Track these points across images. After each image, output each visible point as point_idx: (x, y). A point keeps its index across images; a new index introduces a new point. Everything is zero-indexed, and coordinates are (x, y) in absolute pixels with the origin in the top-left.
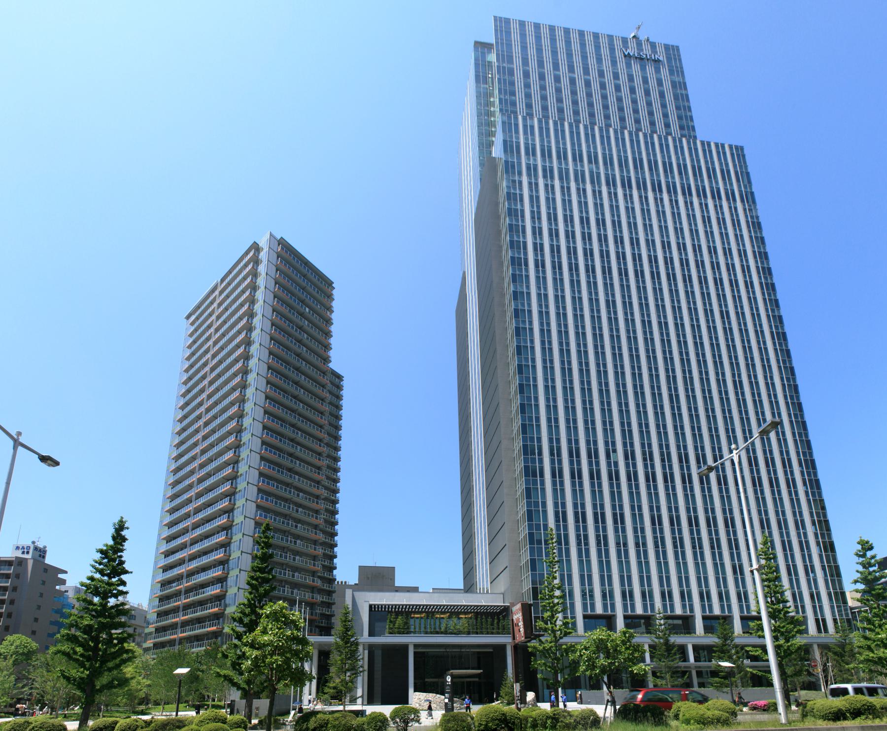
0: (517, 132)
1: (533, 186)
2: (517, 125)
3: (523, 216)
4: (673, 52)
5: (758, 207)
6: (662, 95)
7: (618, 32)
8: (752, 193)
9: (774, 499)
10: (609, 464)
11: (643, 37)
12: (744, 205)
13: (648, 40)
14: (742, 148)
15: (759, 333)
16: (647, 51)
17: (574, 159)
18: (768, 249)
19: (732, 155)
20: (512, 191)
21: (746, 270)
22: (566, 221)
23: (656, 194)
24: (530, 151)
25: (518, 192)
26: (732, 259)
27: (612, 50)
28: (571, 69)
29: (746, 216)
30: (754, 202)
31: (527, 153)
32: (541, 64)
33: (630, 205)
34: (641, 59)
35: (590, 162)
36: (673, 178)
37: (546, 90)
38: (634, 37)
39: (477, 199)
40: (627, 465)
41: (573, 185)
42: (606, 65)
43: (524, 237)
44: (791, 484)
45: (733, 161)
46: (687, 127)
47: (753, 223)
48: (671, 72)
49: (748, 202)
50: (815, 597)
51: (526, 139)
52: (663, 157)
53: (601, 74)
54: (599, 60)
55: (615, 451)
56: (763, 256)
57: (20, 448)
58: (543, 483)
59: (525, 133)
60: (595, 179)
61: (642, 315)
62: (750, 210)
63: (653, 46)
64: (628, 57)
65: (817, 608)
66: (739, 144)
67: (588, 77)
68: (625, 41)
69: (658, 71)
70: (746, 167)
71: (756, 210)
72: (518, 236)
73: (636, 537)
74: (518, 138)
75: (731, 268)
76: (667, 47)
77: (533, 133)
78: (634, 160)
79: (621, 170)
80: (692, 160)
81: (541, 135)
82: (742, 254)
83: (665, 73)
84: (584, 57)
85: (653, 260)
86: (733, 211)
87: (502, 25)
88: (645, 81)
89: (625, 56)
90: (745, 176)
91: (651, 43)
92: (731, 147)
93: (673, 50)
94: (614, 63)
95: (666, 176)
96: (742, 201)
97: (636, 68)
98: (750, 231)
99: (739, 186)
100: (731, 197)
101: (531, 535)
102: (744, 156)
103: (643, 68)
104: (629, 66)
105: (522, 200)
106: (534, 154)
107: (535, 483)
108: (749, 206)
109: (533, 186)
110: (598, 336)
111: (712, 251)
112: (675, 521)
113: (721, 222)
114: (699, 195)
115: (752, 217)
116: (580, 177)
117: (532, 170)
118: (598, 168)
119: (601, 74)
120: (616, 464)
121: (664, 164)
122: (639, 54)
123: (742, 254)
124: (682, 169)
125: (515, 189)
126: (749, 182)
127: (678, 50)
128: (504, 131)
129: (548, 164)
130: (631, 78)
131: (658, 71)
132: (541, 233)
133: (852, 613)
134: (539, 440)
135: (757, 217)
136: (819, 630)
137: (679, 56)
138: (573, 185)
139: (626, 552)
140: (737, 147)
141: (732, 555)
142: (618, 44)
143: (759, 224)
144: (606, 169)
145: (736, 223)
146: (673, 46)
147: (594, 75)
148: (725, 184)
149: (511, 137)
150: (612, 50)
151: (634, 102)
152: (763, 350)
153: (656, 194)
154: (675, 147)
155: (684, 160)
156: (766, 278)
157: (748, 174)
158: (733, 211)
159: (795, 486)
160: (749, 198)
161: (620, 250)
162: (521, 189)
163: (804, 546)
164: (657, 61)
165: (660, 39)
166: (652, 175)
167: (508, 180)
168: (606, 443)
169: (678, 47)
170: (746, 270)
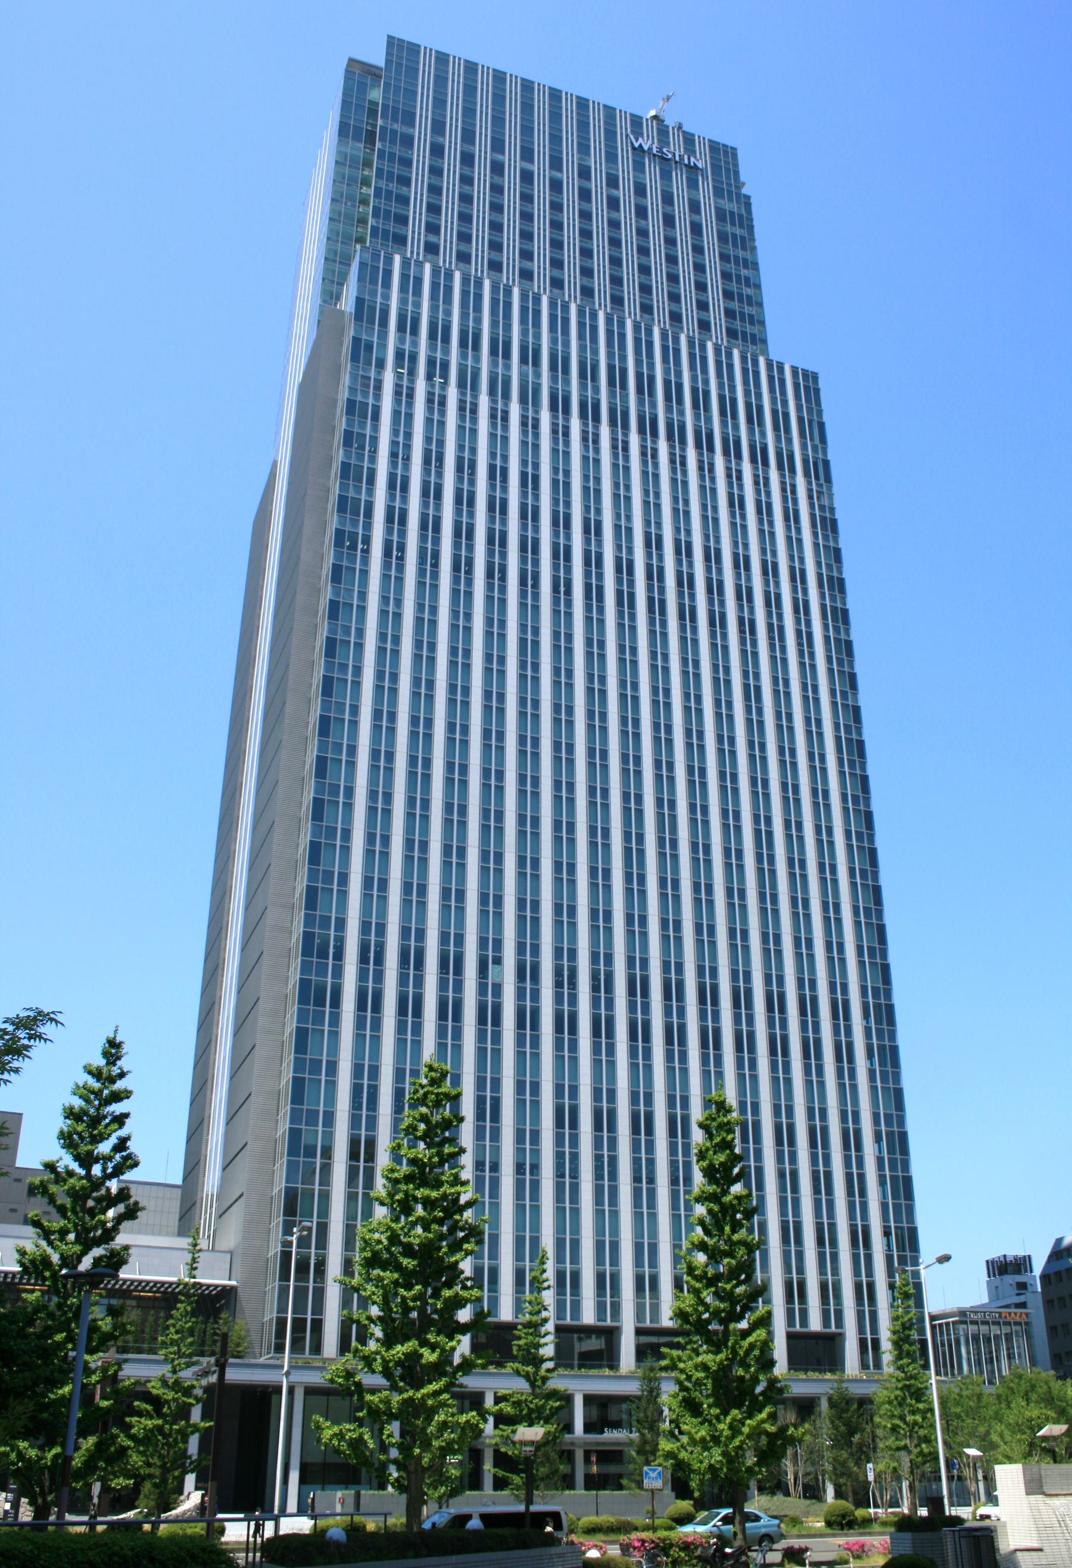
0: (387, 284)
1: (404, 394)
2: (388, 273)
3: (374, 452)
4: (724, 158)
5: (835, 490)
6: (696, 229)
7: (626, 103)
8: (826, 463)
9: (775, 1080)
10: (482, 989)
11: (670, 122)
12: (809, 483)
13: (680, 127)
14: (815, 377)
15: (814, 735)
16: (675, 149)
17: (493, 352)
18: (846, 574)
19: (796, 386)
20: (359, 398)
21: (801, 608)
22: (459, 469)
23: (644, 440)
24: (408, 325)
25: (371, 401)
26: (777, 584)
27: (610, 134)
28: (527, 154)
29: (812, 506)
30: (828, 479)
31: (401, 328)
32: (468, 136)
33: (591, 454)
34: (664, 159)
35: (524, 360)
36: (681, 413)
37: (471, 184)
38: (655, 117)
39: (309, 352)
40: (520, 994)
41: (484, 401)
42: (597, 162)
43: (371, 492)
44: (844, 1053)
45: (797, 397)
46: (746, 325)
47: (823, 519)
48: (718, 192)
49: (817, 478)
50: (865, 1293)
51: (403, 301)
52: (666, 371)
53: (584, 173)
54: (584, 148)
55: (498, 961)
56: (835, 584)
57: (229, 1256)
58: (336, 1020)
59: (403, 289)
60: (529, 396)
61: (791, 557)
62: (820, 493)
63: (689, 140)
64: (639, 151)
65: (867, 1317)
66: (811, 368)
67: (558, 175)
68: (636, 122)
69: (693, 184)
70: (820, 413)
71: (831, 496)
72: (358, 490)
73: (520, 1151)
74: (387, 297)
75: (773, 601)
76: (714, 147)
77: (418, 292)
78: (611, 368)
79: (583, 386)
80: (721, 386)
81: (434, 296)
82: (798, 577)
83: (705, 193)
84: (556, 139)
85: (624, 568)
86: (789, 492)
87: (393, 44)
88: (668, 199)
89: (634, 148)
90: (815, 429)
91: (684, 132)
92: (795, 371)
93: (726, 153)
94: (611, 157)
95: (668, 409)
96: (807, 474)
97: (652, 175)
98: (815, 535)
99: (804, 447)
100: (786, 464)
101: (295, 1135)
102: (817, 391)
103: (666, 176)
104: (639, 167)
105: (376, 417)
106: (415, 331)
107: (319, 1019)
108: (819, 485)
109: (404, 394)
110: (420, 765)
111: (742, 563)
112: (605, 1121)
113: (764, 510)
114: (726, 452)
115: (822, 508)
116: (499, 388)
117: (406, 359)
118: (538, 375)
119: (584, 173)
120: (498, 989)
121: (667, 383)
122: (660, 150)
123: (798, 577)
124: (700, 401)
125: (366, 394)
126: (823, 440)
127: (735, 155)
128: (360, 279)
129: (439, 355)
130: (640, 190)
131: (693, 184)
132: (405, 488)
133: (933, 1327)
134: (341, 924)
135: (832, 510)
136: (864, 1366)
137: (736, 165)
138: (484, 401)
139: (652, 1194)
140: (806, 373)
141: (817, 1204)
142: (623, 128)
143: (834, 522)
144: (554, 379)
145: (791, 517)
146: (724, 146)
147: (569, 177)
148: (778, 438)
149: (374, 293)
150: (610, 134)
151: (670, 241)
152: (818, 770)
153: (644, 440)
154: (692, 356)
155: (706, 382)
156: (837, 629)
157: (822, 426)
158: (789, 492)
159: (851, 1059)
160: (820, 472)
161: (562, 541)
162: (378, 396)
163: (856, 1185)
164: (693, 169)
165: (705, 129)
166: (640, 402)
167: (354, 377)
168: (483, 942)
169: (734, 149)
170: (801, 608)
